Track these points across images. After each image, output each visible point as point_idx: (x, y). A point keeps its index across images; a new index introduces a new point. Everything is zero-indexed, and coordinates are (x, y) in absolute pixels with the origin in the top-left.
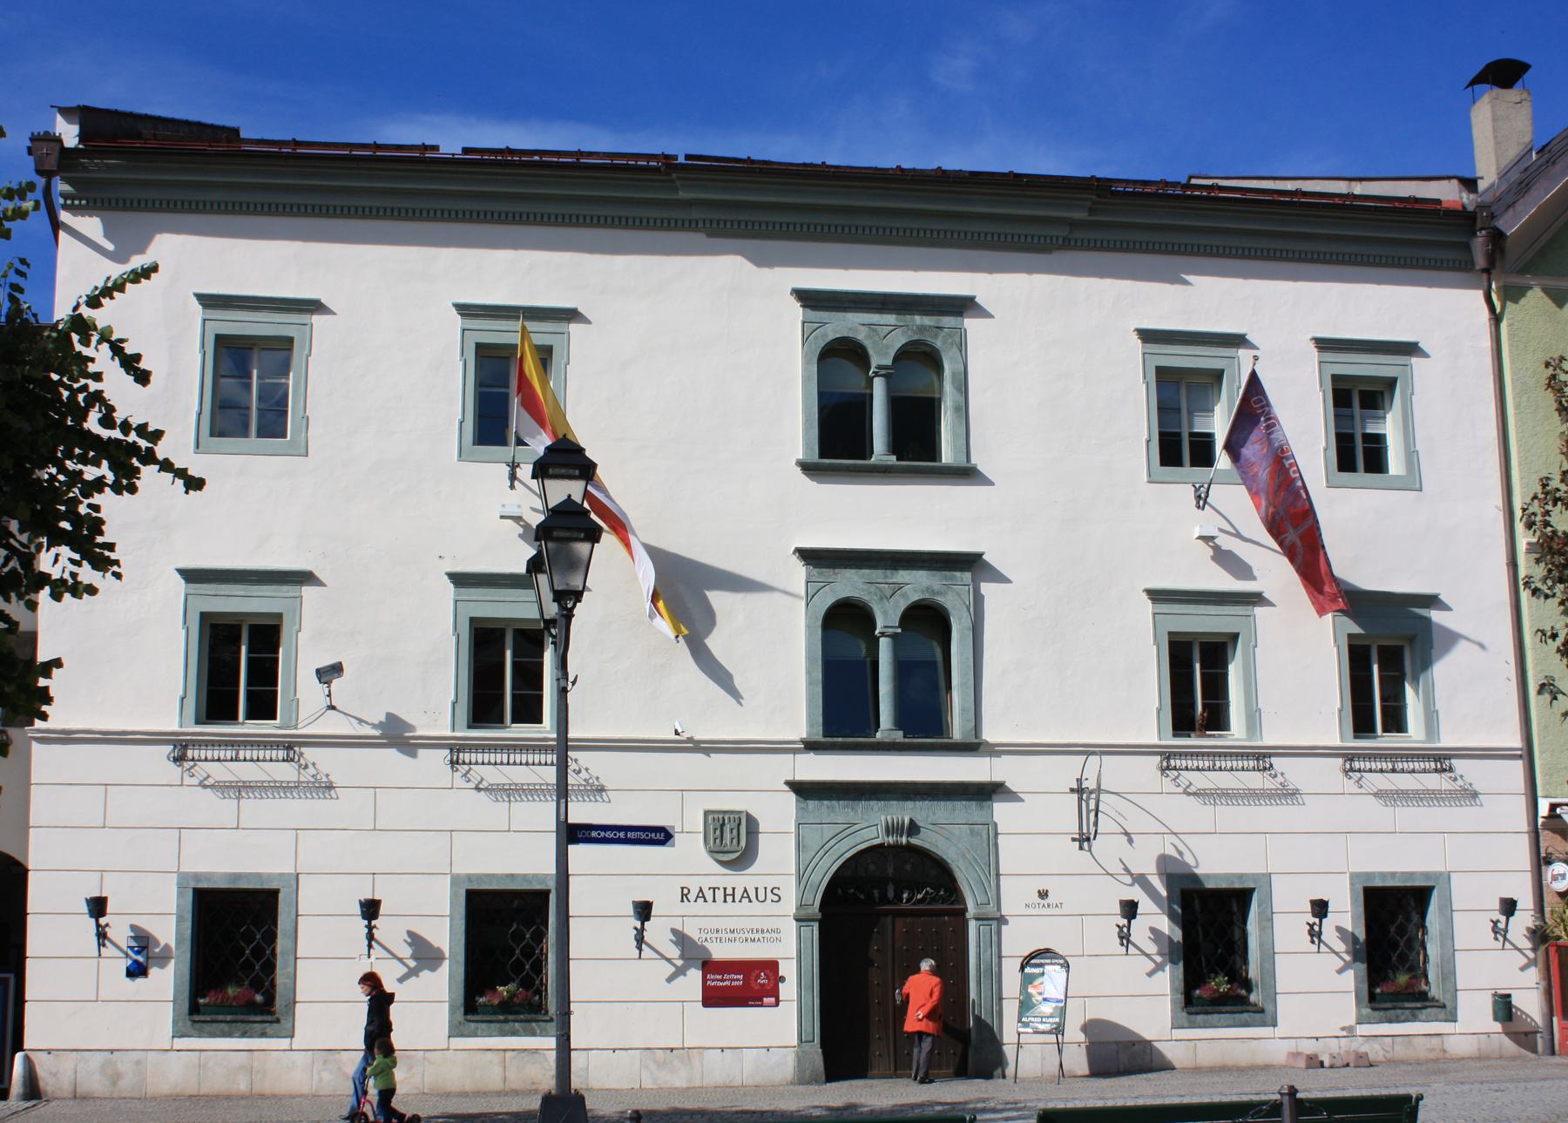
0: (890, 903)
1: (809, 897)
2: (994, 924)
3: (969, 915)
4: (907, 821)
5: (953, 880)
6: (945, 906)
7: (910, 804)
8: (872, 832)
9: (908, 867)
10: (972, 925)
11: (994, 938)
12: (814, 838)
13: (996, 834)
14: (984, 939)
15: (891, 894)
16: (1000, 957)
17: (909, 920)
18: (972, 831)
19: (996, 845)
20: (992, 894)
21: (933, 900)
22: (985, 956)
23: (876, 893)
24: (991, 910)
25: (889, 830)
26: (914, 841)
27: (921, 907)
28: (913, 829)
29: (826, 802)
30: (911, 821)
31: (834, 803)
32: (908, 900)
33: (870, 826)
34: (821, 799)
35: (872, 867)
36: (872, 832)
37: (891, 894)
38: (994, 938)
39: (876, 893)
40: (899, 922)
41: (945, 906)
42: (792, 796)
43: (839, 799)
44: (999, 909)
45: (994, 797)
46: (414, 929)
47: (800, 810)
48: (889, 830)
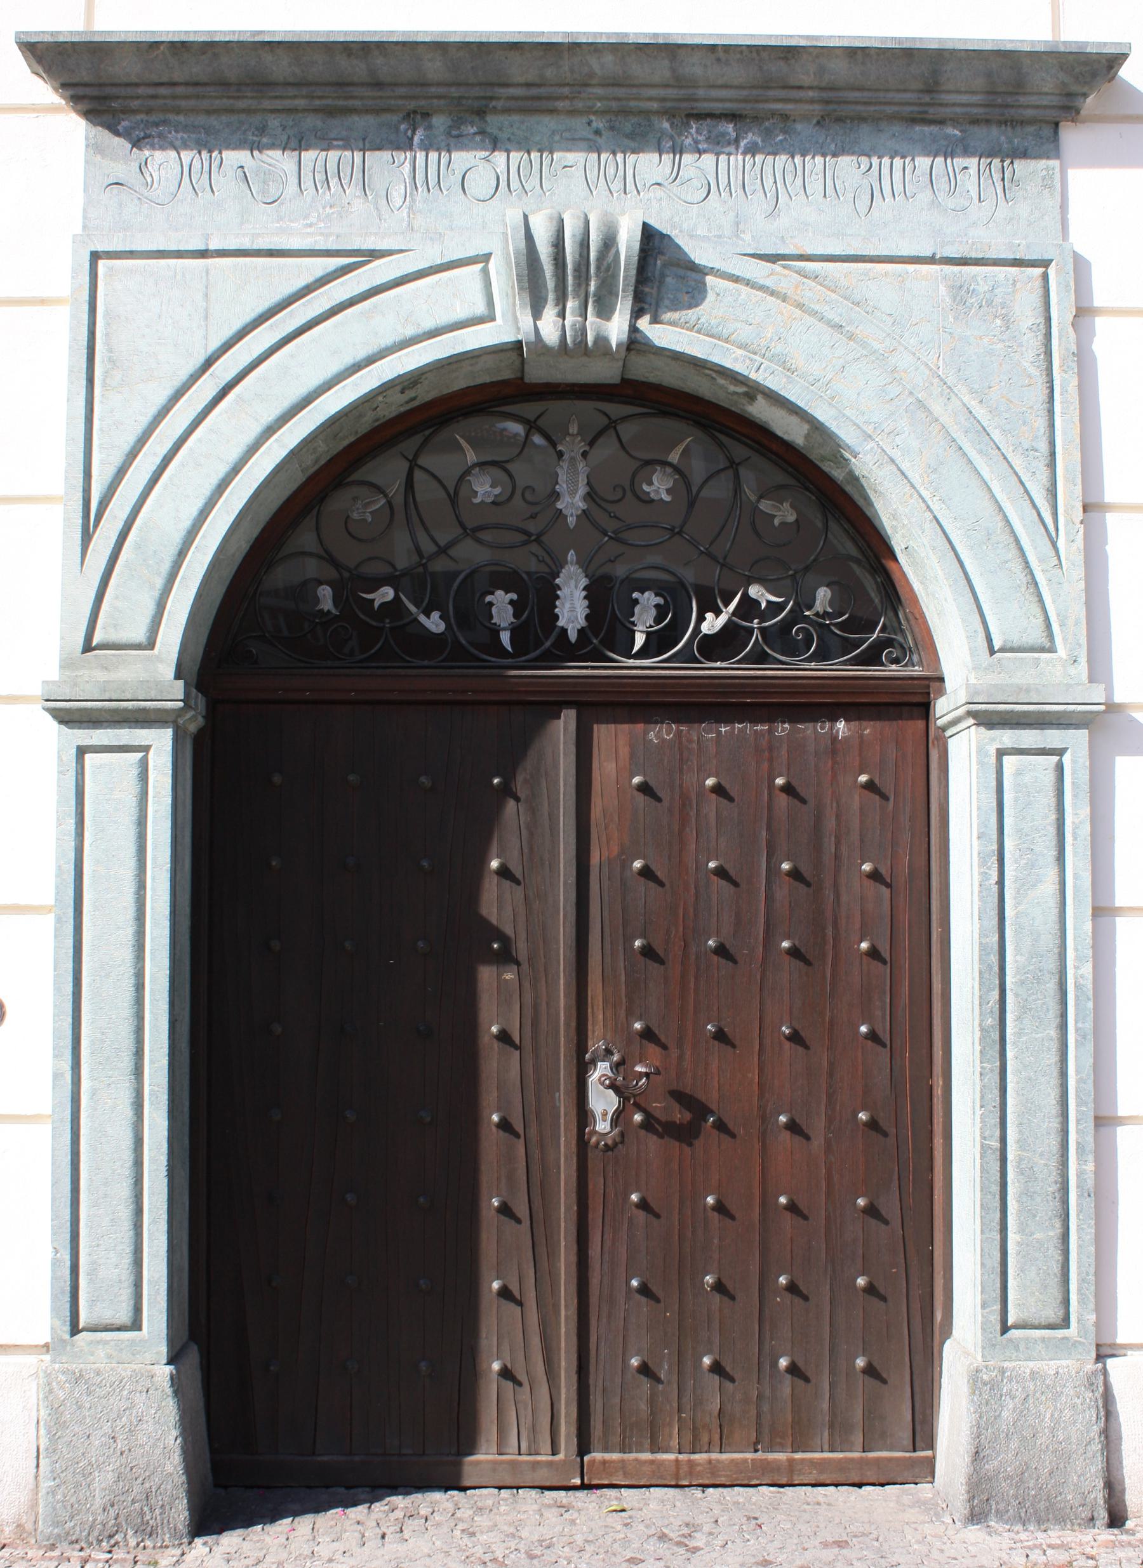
0: (566, 650)
1: (351, 1537)
2: (1076, 741)
3: (943, 708)
4: (628, 241)
5: (874, 549)
6: (837, 669)
7: (649, 165)
8: (460, 294)
9: (659, 486)
10: (966, 755)
11: (1077, 815)
12: (166, 322)
13: (1083, 313)
14: (1030, 820)
15: (572, 610)
16: (1103, 912)
17: (660, 733)
18: (960, 293)
19: (1084, 362)
20: (1065, 597)
21: (783, 639)
22: (1030, 907)
23: (501, 606)
24: (1058, 679)
25: (544, 274)
26: (664, 334)
27: (717, 668)
28: (661, 271)
29: (234, 157)
30: (649, 234)
31: (280, 161)
32: (658, 643)
33: (444, 262)
34: (208, 141)
35: (484, 488)
36: (460, 294)
37: (572, 610)
38: (1077, 815)
39: (501, 606)
40: (611, 739)
41: (837, 669)
42: (74, 127)
43: (298, 143)
44: (1098, 664)
45: (1071, 137)
46: (64, 21)
47: (94, 148)
48: (544, 274)
